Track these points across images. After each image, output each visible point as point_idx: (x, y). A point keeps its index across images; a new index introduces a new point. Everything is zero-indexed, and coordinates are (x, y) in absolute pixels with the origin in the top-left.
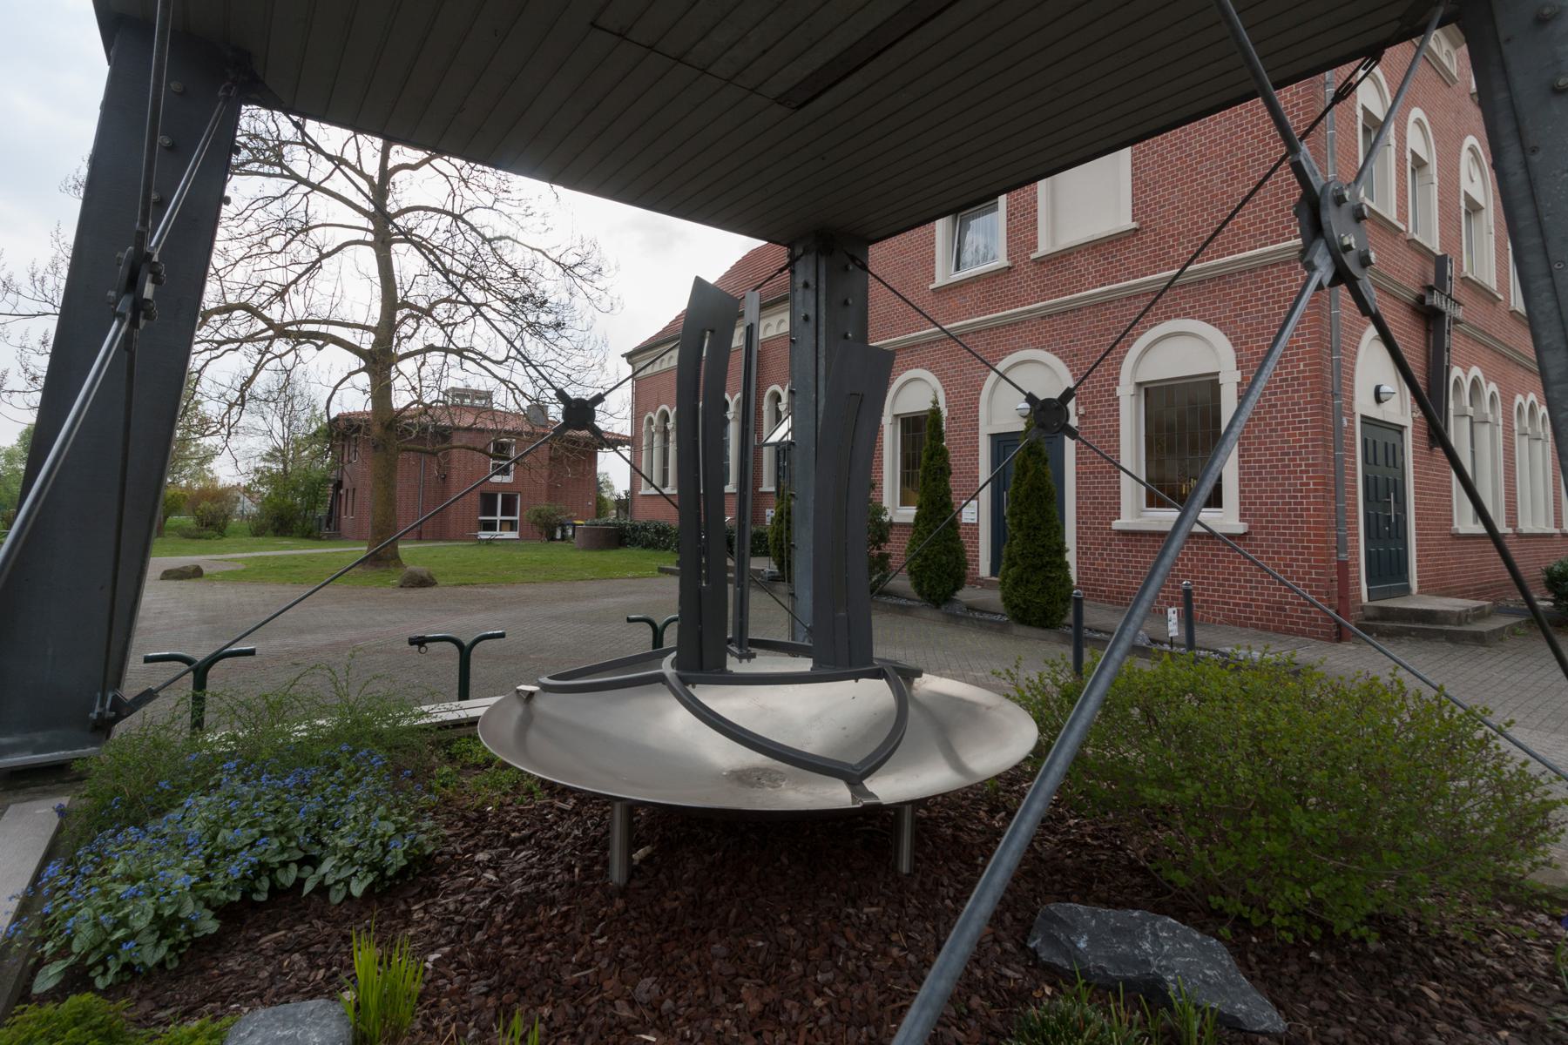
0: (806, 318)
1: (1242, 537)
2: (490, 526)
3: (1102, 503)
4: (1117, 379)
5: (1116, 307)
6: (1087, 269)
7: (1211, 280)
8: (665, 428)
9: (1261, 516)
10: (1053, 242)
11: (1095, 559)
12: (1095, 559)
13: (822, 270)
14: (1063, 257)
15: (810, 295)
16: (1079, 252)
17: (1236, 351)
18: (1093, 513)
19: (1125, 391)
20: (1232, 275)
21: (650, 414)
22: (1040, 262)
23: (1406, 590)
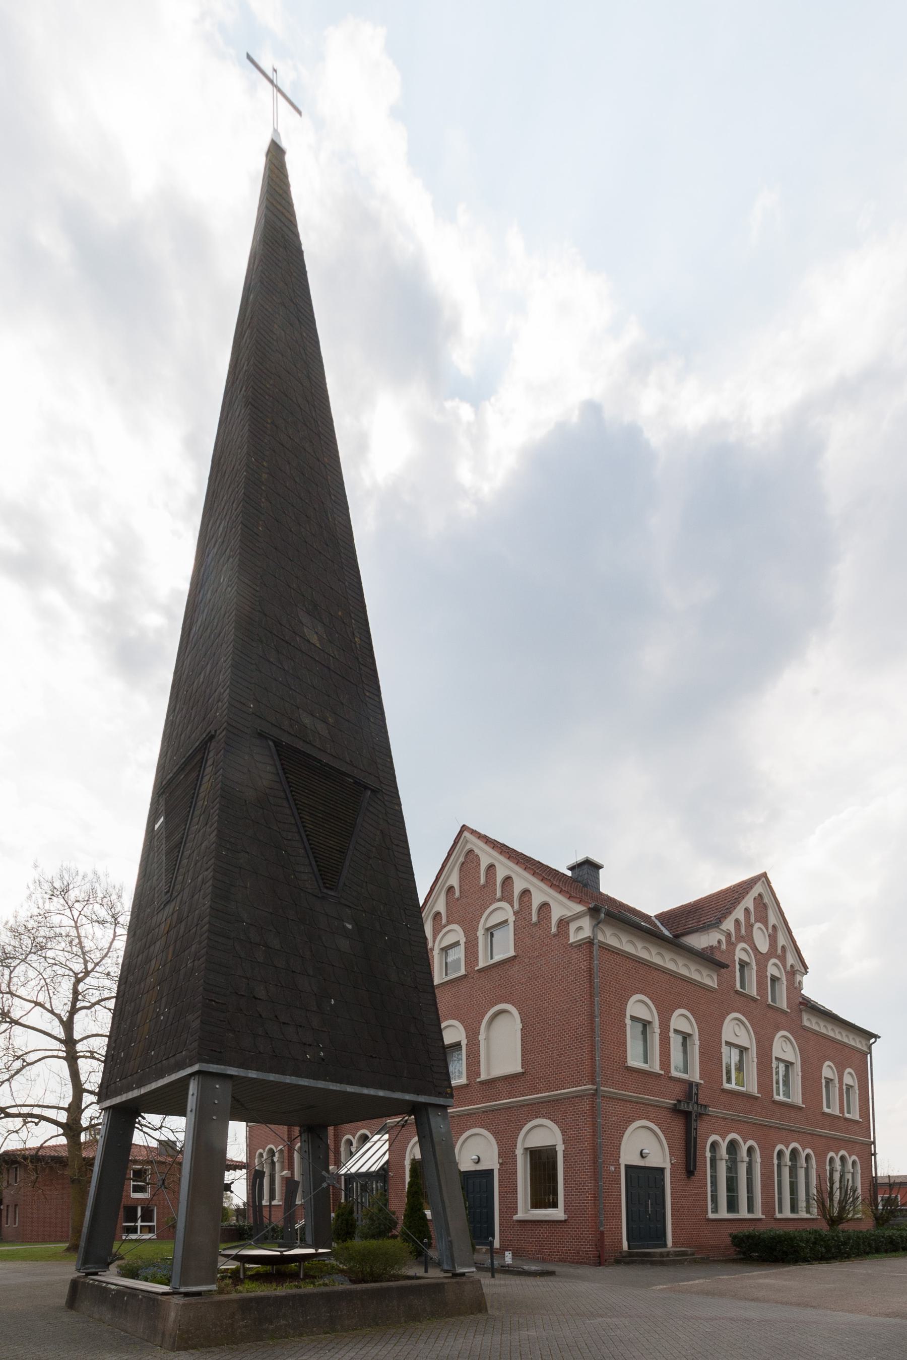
0: (305, 1151)
1: (565, 1221)
2: (134, 1230)
3: (510, 1207)
4: (516, 1146)
5: (515, 1110)
6: (502, 1090)
7: (553, 1101)
8: (273, 1160)
9: (572, 1212)
10: (489, 1074)
11: (508, 1235)
12: (508, 1235)
13: (310, 1137)
14: (492, 1081)
15: (307, 1144)
16: (499, 1080)
17: (563, 1135)
18: (506, 1212)
19: (519, 1152)
20: (561, 1100)
21: (261, 1151)
22: (482, 1083)
23: (665, 1245)
